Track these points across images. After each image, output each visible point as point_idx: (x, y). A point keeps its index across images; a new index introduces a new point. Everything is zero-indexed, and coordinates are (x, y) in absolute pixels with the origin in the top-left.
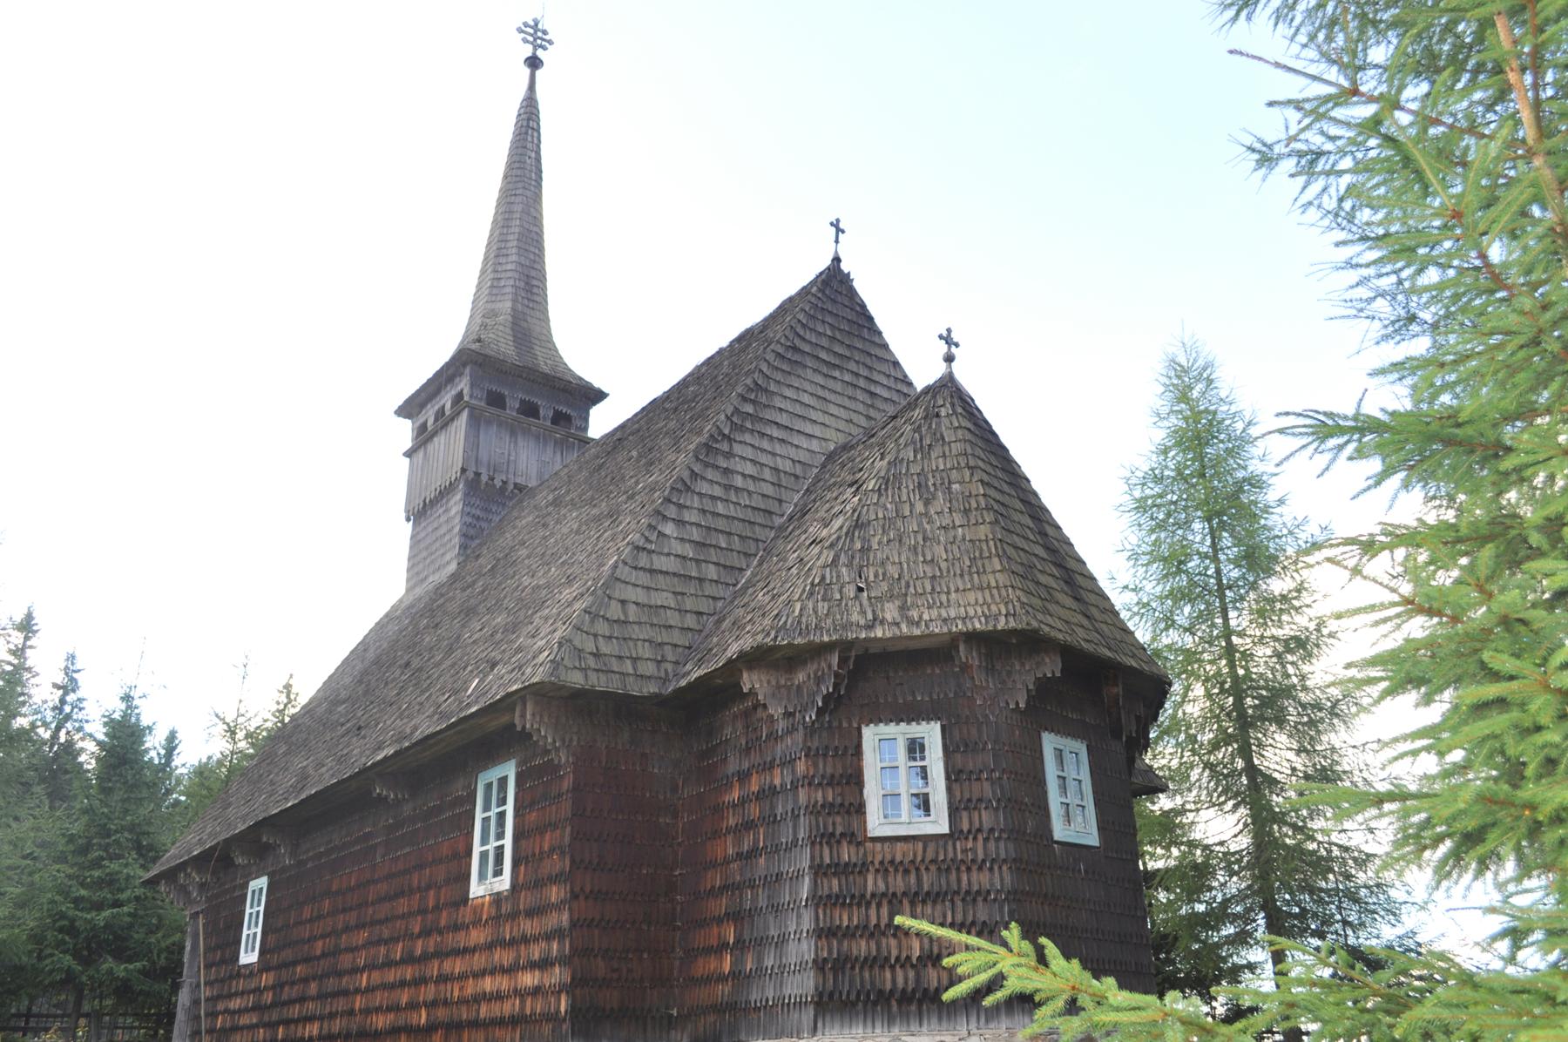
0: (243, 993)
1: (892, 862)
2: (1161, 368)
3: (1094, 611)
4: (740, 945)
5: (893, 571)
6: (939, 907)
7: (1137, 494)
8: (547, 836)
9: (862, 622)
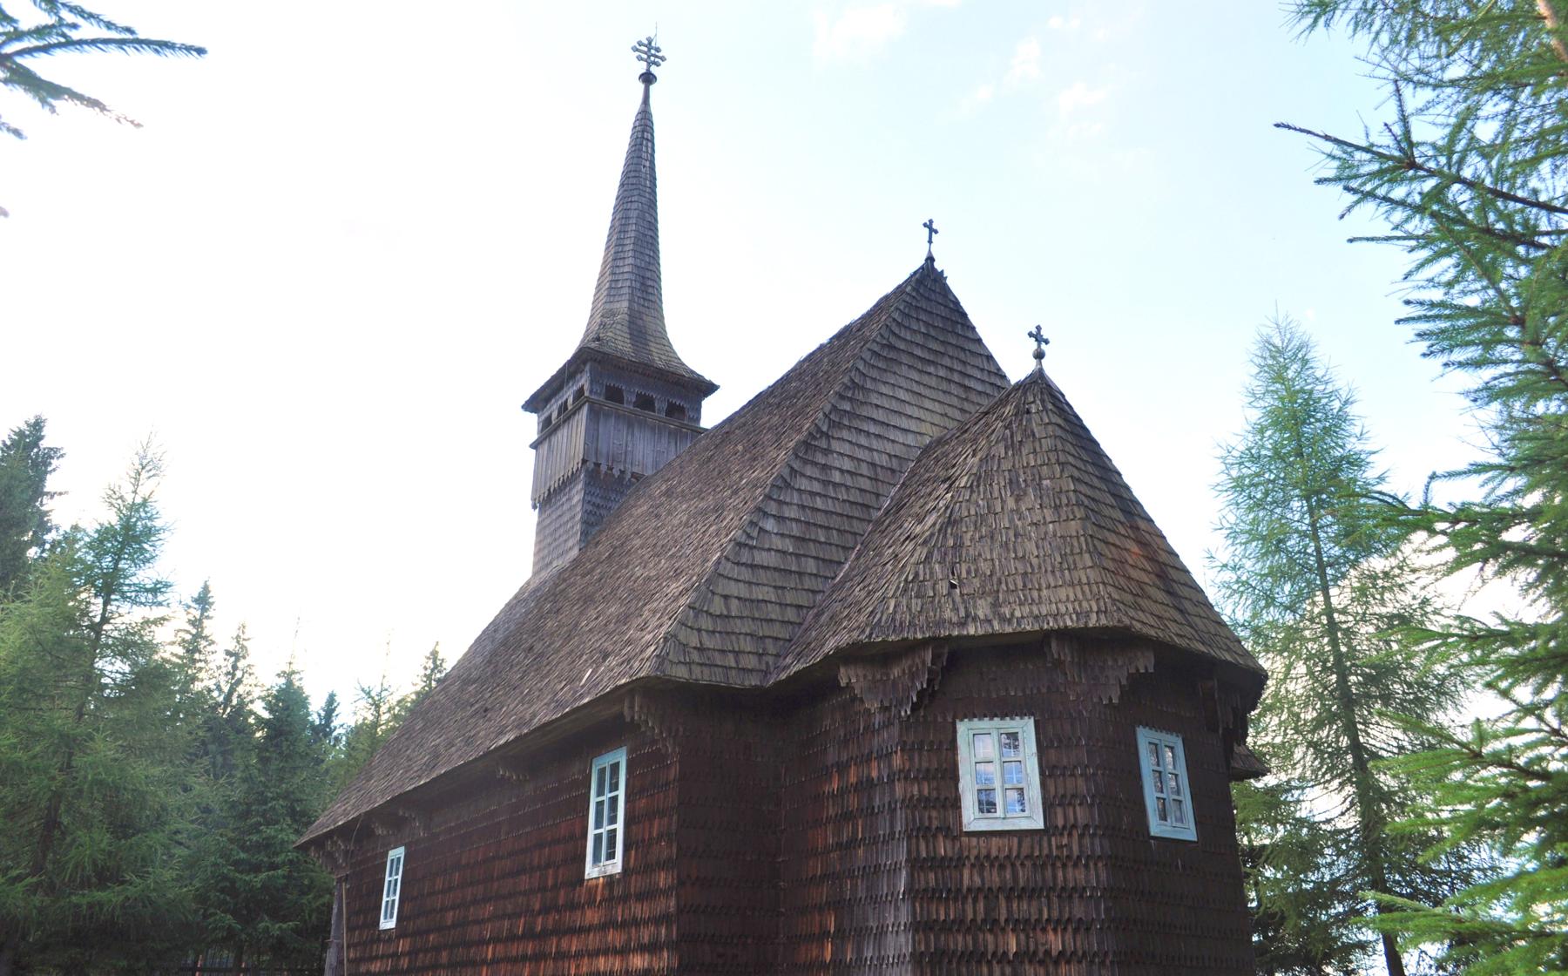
0: (383, 957)
1: (988, 857)
2: (1254, 349)
3: (1187, 605)
4: (841, 935)
5: (985, 567)
6: (1034, 903)
7: (1234, 473)
8: (656, 822)
9: (955, 619)
